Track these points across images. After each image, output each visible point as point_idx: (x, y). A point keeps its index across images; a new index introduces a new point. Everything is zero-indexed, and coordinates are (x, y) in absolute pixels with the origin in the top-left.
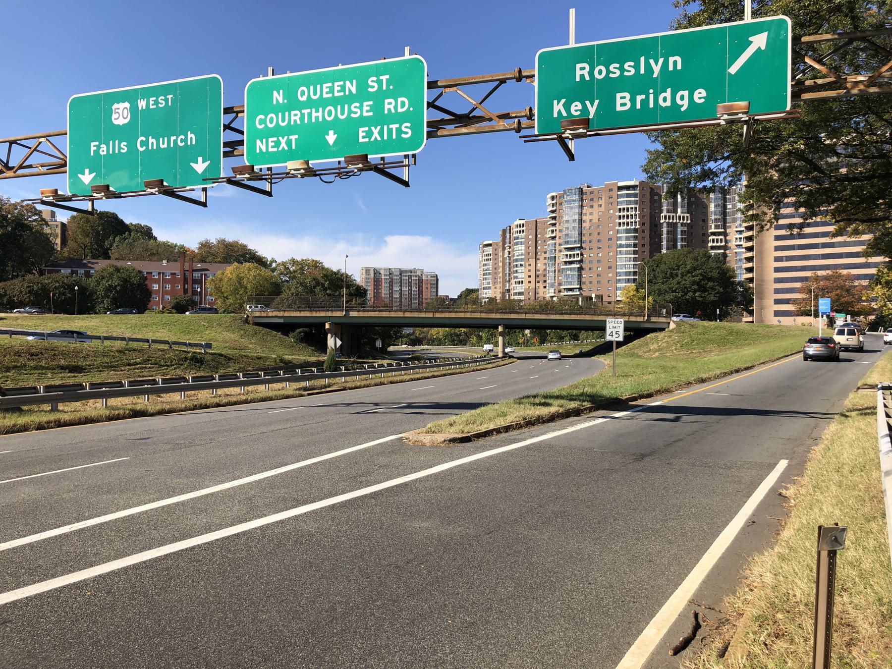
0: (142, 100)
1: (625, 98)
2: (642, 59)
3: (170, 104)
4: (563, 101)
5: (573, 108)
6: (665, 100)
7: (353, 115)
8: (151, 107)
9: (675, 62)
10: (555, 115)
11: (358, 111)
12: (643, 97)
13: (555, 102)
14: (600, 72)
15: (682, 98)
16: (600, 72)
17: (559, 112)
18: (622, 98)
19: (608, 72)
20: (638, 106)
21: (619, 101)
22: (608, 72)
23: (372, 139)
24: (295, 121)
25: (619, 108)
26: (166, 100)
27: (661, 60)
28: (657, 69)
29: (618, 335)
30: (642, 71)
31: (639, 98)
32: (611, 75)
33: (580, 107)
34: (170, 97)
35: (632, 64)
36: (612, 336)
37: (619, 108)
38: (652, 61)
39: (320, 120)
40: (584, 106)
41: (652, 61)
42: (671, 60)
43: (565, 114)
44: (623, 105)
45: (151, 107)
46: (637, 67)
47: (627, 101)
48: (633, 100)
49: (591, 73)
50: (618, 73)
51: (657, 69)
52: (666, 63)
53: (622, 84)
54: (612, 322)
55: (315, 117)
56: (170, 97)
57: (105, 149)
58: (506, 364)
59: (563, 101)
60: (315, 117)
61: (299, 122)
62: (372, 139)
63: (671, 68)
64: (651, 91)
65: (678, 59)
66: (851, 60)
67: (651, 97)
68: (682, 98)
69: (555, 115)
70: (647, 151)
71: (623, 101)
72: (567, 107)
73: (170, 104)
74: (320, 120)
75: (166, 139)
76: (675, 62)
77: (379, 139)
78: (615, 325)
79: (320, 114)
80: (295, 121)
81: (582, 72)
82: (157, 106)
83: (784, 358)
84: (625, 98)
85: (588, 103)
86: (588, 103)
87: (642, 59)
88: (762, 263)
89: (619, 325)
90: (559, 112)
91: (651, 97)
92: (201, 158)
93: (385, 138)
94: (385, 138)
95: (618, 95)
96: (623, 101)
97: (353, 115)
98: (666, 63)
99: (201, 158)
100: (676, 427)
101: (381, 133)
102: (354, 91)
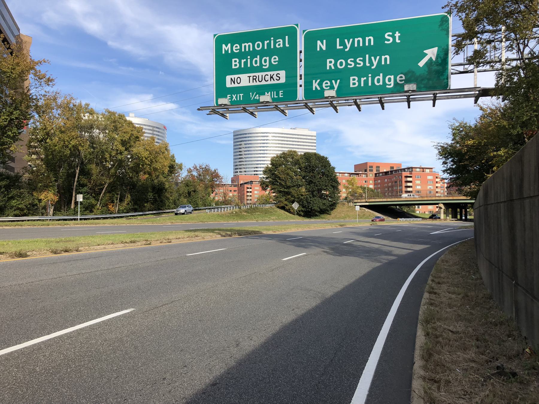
2: (367, 56)
4: (318, 81)
6: (378, 81)
9: (386, 59)
13: (314, 81)
14: (341, 64)
15: (390, 80)
16: (341, 64)
17: (316, 88)
19: (347, 64)
20: (362, 85)
21: (352, 82)
22: (347, 64)
23: (233, 100)
24: (330, 66)
38: (373, 58)
40: (331, 83)
44: (354, 84)
46: (364, 61)
49: (335, 65)
57: (281, 43)
59: (318, 81)
61: (333, 68)
62: (233, 100)
64: (370, 75)
66: (57, 105)
67: (370, 79)
68: (390, 80)
69: (314, 89)
70: (359, 109)
75: (367, 44)
77: (236, 100)
80: (330, 66)
81: (330, 64)
85: (333, 81)
86: (333, 81)
87: (367, 56)
90: (316, 88)
91: (370, 79)
93: (238, 100)
94: (238, 100)
96: (354, 82)
101: (236, 97)
102: (319, 43)
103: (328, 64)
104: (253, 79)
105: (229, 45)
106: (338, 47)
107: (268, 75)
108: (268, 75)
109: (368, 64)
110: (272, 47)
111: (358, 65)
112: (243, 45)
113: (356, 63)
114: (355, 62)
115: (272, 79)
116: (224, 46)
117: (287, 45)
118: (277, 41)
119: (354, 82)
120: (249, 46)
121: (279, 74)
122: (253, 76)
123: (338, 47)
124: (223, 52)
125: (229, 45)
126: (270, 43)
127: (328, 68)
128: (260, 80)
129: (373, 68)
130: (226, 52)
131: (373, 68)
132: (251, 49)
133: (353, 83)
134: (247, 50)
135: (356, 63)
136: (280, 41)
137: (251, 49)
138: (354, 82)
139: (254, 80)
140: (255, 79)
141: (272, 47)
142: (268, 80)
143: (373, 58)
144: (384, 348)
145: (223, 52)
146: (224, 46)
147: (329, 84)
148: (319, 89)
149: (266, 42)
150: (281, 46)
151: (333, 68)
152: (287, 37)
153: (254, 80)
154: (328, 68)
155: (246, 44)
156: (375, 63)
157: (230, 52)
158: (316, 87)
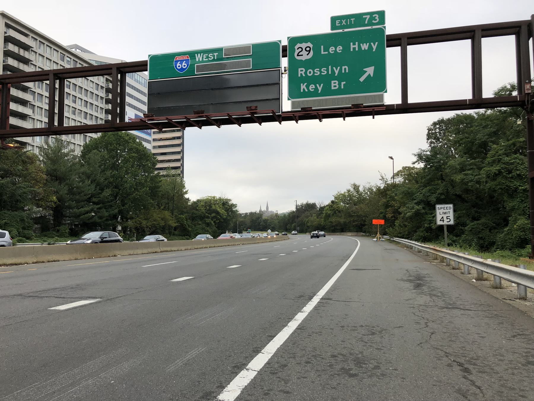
0: (365, 44)
1: (336, 83)
2: (330, 67)
4: (306, 84)
5: (310, 88)
9: (345, 69)
10: (302, 91)
13: (302, 84)
14: (310, 72)
16: (310, 72)
17: (304, 89)
18: (334, 83)
19: (314, 73)
20: (342, 87)
21: (333, 85)
22: (314, 73)
24: (301, 74)
25: (333, 88)
27: (339, 68)
28: (337, 72)
29: (449, 220)
30: (330, 73)
32: (315, 74)
33: (314, 87)
35: (325, 69)
36: (443, 221)
37: (333, 88)
38: (334, 68)
39: (357, 49)
40: (316, 87)
41: (334, 68)
42: (343, 67)
43: (306, 90)
44: (335, 86)
47: (337, 84)
48: (340, 84)
49: (306, 73)
50: (319, 73)
51: (337, 72)
52: (341, 69)
54: (441, 208)
55: (353, 48)
58: (168, 251)
59: (306, 84)
60: (353, 48)
61: (304, 75)
62: (342, 24)
63: (343, 72)
65: (346, 67)
69: (302, 91)
71: (335, 85)
72: (307, 87)
74: (357, 49)
76: (345, 69)
78: (445, 211)
79: (356, 46)
80: (301, 74)
81: (301, 72)
83: (165, 253)
84: (336, 83)
85: (318, 85)
86: (318, 85)
87: (330, 67)
89: (449, 210)
90: (304, 89)
95: (333, 82)
98: (341, 69)
100: (515, 298)
103: (300, 73)
106: (322, 53)
111: (322, 74)
113: (321, 72)
123: (322, 53)
127: (299, 76)
135: (321, 72)
144: (337, 280)
148: (306, 90)
151: (304, 75)
154: (299, 76)
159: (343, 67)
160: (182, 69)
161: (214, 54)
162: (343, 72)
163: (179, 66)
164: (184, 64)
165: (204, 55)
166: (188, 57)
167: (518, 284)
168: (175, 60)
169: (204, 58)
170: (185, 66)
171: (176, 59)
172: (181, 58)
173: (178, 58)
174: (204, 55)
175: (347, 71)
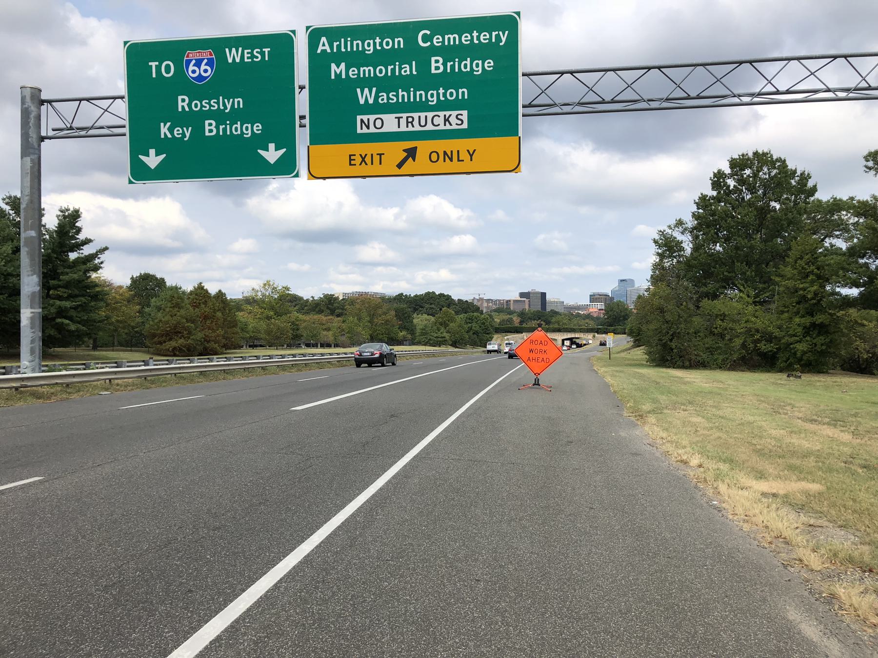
2: (221, 98)
3: (267, 59)
4: (168, 124)
7: (204, 109)
8: (246, 60)
9: (239, 102)
11: (395, 99)
12: (224, 126)
13: (162, 124)
14: (196, 106)
16: (196, 106)
17: (165, 133)
19: (202, 106)
22: (202, 106)
24: (183, 107)
26: (262, 54)
27: (231, 100)
31: (221, 127)
34: (266, 50)
38: (226, 100)
40: (172, 134)
42: (236, 100)
45: (246, 60)
46: (218, 103)
49: (189, 105)
53: (210, 115)
56: (266, 50)
57: (408, 69)
59: (168, 124)
61: (187, 109)
63: (236, 107)
69: (163, 136)
72: (171, 130)
73: (267, 59)
76: (463, 93)
80: (183, 107)
81: (183, 104)
82: (252, 60)
85: (185, 129)
86: (185, 129)
87: (221, 98)
88: (313, 347)
92: (273, 145)
97: (204, 109)
99: (273, 145)
103: (180, 104)
104: (408, 122)
105: (343, 65)
107: (439, 116)
108: (439, 116)
109: (222, 108)
110: (397, 74)
112: (362, 69)
114: (209, 104)
115: (447, 122)
116: (333, 66)
117: (415, 73)
118: (403, 66)
119: (210, 128)
120: (369, 71)
121: (462, 115)
122: (407, 118)
124: (333, 77)
125: (343, 65)
126: (454, 66)
127: (180, 109)
128: (423, 123)
129: (226, 111)
130: (338, 76)
131: (226, 111)
132: (372, 75)
133: (209, 130)
134: (367, 76)
136: (406, 67)
137: (372, 75)
138: (437, 65)
139: (410, 124)
140: (412, 123)
141: (397, 74)
142: (439, 125)
143: (226, 100)
145: (333, 77)
146: (333, 66)
147: (181, 132)
148: (169, 136)
149: (390, 68)
150: (408, 73)
151: (187, 109)
152: (414, 63)
153: (410, 124)
154: (180, 109)
155: (365, 68)
156: (229, 107)
157: (344, 76)
158: (165, 133)
159: (236, 100)
160: (200, 78)
161: (264, 50)
162: (236, 107)
163: (194, 72)
164: (203, 67)
165: (246, 51)
166: (211, 55)
167: (171, 374)
168: (185, 58)
169: (246, 58)
170: (206, 71)
171: (188, 56)
172: (198, 55)
173: (191, 55)
174: (246, 51)
175: (466, 97)
